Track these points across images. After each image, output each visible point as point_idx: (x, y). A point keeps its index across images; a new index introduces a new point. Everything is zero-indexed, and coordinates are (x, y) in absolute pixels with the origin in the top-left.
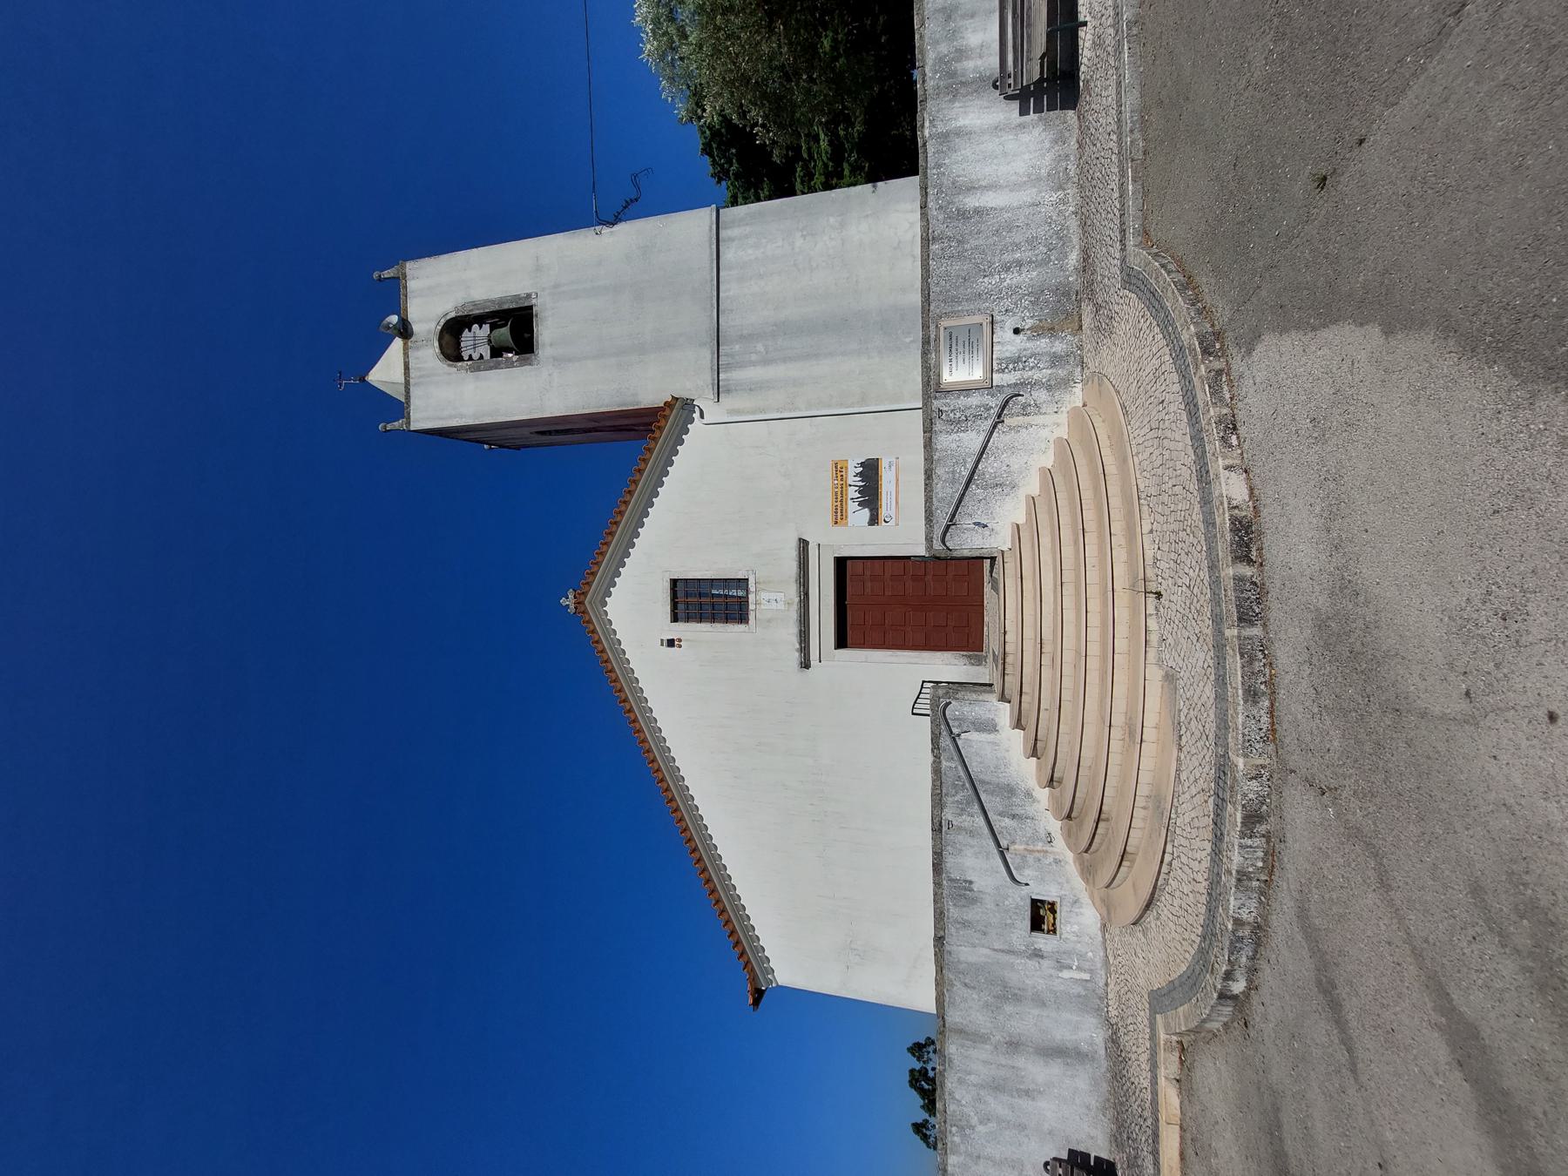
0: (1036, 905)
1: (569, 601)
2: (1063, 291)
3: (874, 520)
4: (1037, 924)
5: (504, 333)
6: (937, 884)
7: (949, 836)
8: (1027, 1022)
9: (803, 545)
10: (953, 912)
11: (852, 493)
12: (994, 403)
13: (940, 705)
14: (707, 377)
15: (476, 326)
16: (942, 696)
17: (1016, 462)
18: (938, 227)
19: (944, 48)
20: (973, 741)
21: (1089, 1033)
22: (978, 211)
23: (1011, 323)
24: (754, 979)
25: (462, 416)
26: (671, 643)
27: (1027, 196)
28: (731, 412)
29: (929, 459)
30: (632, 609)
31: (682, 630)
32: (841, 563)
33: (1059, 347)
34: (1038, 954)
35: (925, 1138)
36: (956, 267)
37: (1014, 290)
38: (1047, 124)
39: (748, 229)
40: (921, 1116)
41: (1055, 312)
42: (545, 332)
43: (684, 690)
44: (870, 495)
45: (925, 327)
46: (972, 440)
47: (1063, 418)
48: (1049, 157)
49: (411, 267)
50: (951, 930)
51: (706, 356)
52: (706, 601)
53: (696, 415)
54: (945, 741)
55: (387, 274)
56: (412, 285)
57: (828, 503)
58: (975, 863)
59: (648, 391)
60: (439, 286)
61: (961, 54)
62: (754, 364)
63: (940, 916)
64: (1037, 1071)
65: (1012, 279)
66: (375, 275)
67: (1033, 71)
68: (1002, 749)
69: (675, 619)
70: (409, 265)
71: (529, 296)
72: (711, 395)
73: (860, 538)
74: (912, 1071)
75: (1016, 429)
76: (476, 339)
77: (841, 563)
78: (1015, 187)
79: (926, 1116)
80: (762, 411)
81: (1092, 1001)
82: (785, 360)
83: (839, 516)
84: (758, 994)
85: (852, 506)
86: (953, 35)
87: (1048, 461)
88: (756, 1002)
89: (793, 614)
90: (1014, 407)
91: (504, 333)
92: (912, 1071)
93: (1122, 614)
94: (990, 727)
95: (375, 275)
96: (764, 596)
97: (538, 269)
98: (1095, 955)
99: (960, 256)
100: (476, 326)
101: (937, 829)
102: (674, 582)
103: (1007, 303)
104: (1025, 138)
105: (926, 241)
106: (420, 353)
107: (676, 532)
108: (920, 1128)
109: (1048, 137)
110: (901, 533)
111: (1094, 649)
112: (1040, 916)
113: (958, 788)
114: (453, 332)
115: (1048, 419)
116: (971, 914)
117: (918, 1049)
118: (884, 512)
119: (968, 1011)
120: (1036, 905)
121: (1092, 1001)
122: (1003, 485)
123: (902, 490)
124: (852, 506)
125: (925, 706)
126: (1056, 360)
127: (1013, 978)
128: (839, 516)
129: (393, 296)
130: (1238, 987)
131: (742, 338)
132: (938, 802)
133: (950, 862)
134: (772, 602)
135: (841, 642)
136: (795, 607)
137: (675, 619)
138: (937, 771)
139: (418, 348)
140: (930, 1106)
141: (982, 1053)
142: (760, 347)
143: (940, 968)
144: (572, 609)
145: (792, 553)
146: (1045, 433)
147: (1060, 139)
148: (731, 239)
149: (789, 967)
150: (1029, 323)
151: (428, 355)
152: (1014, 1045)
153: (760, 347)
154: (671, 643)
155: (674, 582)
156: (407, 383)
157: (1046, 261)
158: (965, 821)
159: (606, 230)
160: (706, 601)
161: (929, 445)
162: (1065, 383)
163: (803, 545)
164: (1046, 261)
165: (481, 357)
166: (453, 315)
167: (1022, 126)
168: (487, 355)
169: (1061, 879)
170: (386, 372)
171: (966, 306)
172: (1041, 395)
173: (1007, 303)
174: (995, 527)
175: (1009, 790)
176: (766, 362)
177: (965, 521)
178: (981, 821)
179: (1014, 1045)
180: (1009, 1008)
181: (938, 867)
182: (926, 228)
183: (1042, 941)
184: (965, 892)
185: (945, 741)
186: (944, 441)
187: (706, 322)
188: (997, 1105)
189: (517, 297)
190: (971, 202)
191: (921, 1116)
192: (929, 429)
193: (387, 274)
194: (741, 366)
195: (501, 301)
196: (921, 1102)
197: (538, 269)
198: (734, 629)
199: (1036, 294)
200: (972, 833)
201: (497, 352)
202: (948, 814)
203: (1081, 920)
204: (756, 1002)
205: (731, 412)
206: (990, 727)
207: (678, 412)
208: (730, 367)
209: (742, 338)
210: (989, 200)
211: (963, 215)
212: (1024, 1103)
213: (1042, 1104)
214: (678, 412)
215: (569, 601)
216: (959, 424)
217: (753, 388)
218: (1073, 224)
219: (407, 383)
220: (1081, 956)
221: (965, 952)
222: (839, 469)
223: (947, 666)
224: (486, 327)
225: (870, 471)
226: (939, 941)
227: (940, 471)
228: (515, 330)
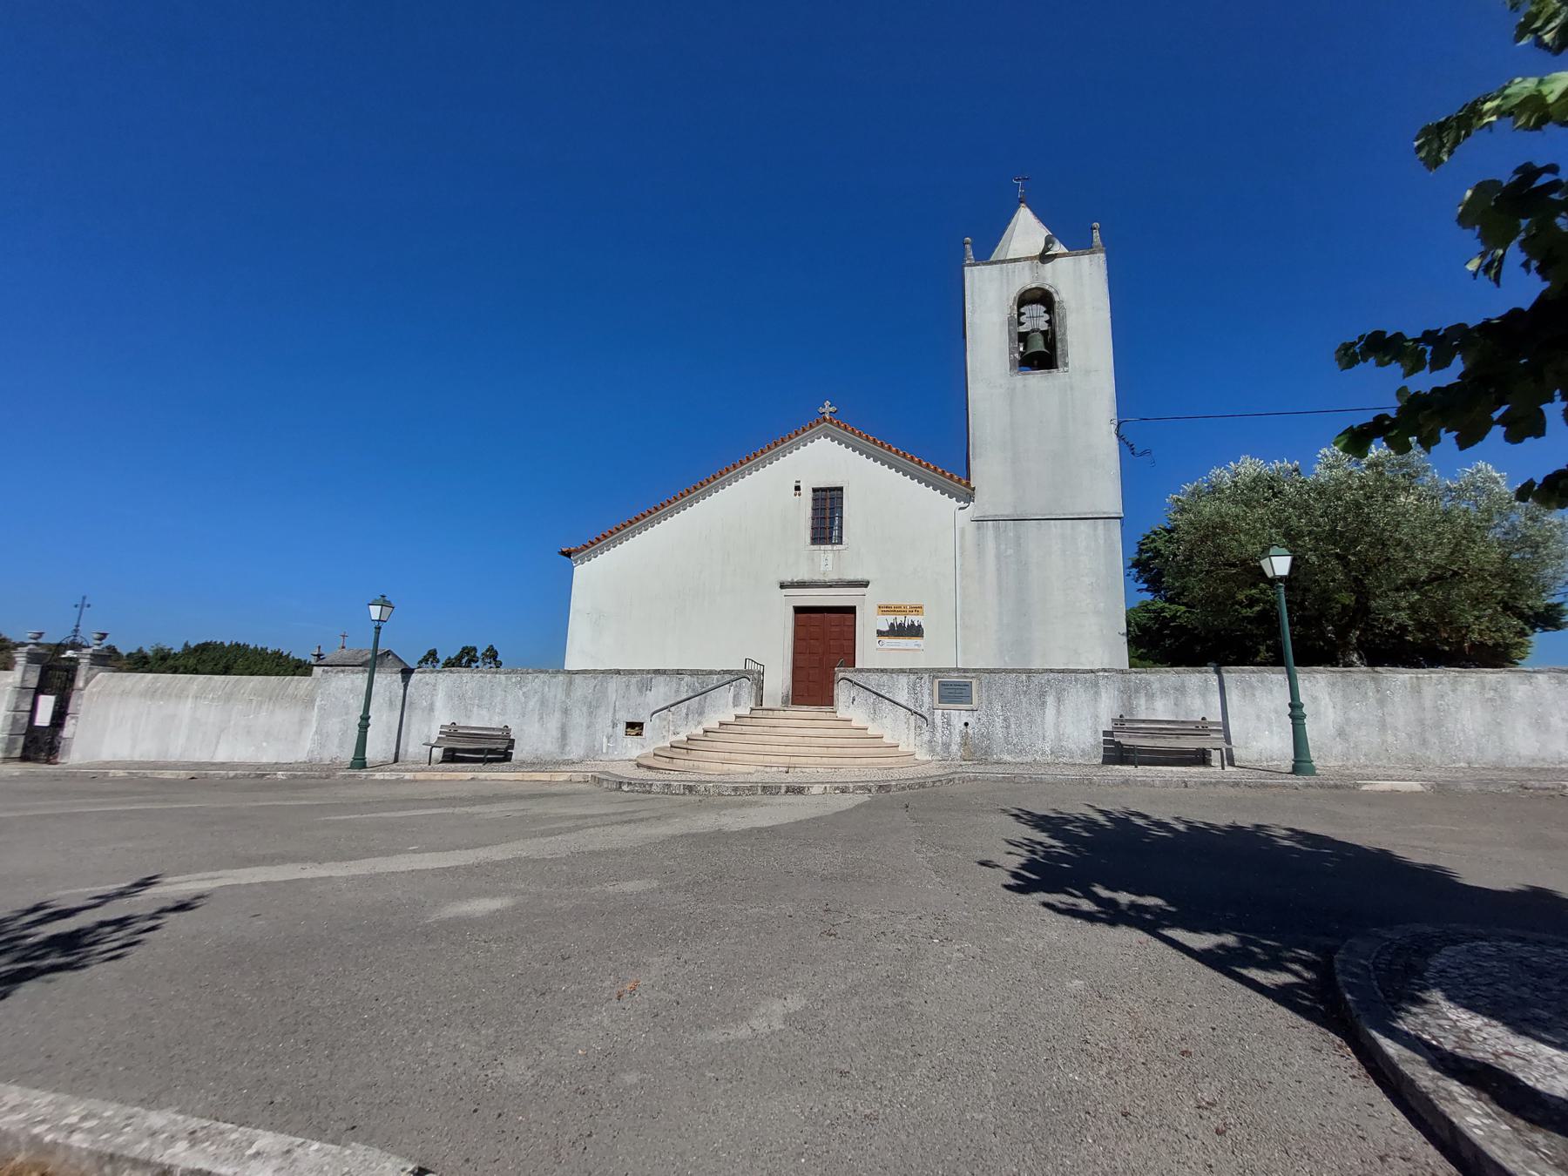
0: (641, 725)
1: (828, 408)
2: (988, 751)
3: (880, 633)
4: (631, 725)
5: (1038, 345)
6: (648, 672)
7: (675, 678)
8: (578, 718)
9: (865, 584)
10: (634, 679)
11: (900, 619)
12: (924, 711)
13: (753, 677)
14: (991, 512)
15: (1047, 317)
16: (753, 677)
17: (888, 722)
18: (1036, 679)
19: (1156, 686)
20: (727, 694)
21: (575, 751)
22: (1044, 703)
23: (971, 721)
24: (577, 551)
25: (974, 312)
26: (797, 488)
27: (1051, 733)
28: (963, 531)
29: (893, 671)
30: (822, 458)
31: (807, 496)
32: (851, 610)
33: (954, 748)
34: (614, 725)
35: (425, 660)
36: (1009, 689)
37: (992, 723)
38: (1095, 747)
39: (1102, 542)
40: (442, 658)
41: (975, 746)
42: (1037, 380)
43: (770, 492)
44: (897, 631)
45: (975, 670)
46: (903, 697)
47: (911, 749)
48: (1073, 747)
49: (1100, 258)
50: (625, 679)
51: (1007, 511)
52: (827, 515)
53: (962, 504)
54: (727, 677)
55: (1096, 234)
56: (1085, 259)
57: (894, 602)
58: (661, 692)
59: (986, 468)
60: (1082, 284)
61: (1150, 697)
62: (998, 548)
63: (631, 672)
64: (553, 723)
65: (999, 722)
66: (1096, 225)
67: (1126, 740)
68: (724, 708)
69: (814, 490)
70: (1102, 256)
71: (1066, 365)
72: (977, 515)
73: (868, 624)
74: (475, 649)
75: (907, 722)
76: (1036, 318)
77: (851, 610)
78: (1057, 725)
79: (443, 661)
80: (962, 554)
81: (592, 753)
82: (998, 570)
83: (885, 609)
84: (568, 554)
85: (891, 619)
86: (1164, 692)
87: (887, 740)
88: (563, 553)
89: (817, 577)
90: (920, 721)
91: (1038, 345)
92: (475, 649)
93: (781, 760)
94: (736, 704)
95: (1096, 225)
96: (830, 556)
97: (1087, 372)
98: (615, 755)
99: (1016, 693)
100: (1047, 317)
101: (679, 672)
102: (841, 489)
103: (984, 719)
104: (1088, 733)
105: (1029, 672)
106: (1027, 272)
107: (876, 488)
108: (432, 656)
109: (1087, 747)
110: (870, 650)
111: (768, 748)
112: (635, 727)
113: (702, 684)
114: (1042, 298)
115: (912, 741)
116: (633, 688)
117: (492, 655)
118: (886, 640)
119: (582, 687)
120: (641, 725)
121: (592, 753)
122: (875, 713)
123: (902, 652)
124: (891, 619)
125: (750, 666)
126: (946, 746)
127: (601, 711)
128: (885, 609)
129: (1078, 244)
130: (625, 788)
131: (1018, 537)
132: (694, 673)
133: (661, 678)
134: (826, 562)
135: (799, 610)
136: (822, 578)
137: (814, 490)
138: (711, 672)
139: (1031, 269)
140: (451, 664)
141: (561, 695)
142: (1010, 552)
143: (603, 672)
144: (821, 410)
145: (859, 577)
146: (904, 737)
147: (1084, 753)
148: (1095, 529)
149: (587, 573)
150: (970, 732)
151: (1025, 278)
152: (566, 712)
153: (1010, 552)
154: (797, 488)
155: (841, 489)
156: (1003, 262)
157: (1008, 743)
158: (684, 688)
159: (1113, 428)
160: (827, 515)
161: (902, 671)
162: (932, 751)
163: (865, 584)
164: (1008, 743)
165: (1021, 324)
166: (1056, 298)
167: (1096, 732)
168: (1022, 329)
169: (655, 738)
170: (1026, 232)
171: (985, 695)
172: (926, 737)
173: (984, 719)
174: (849, 705)
175: (701, 714)
176: (998, 557)
177: (854, 691)
178: (684, 696)
179: (566, 712)
180: (585, 709)
181: (657, 672)
182: (1037, 672)
183: (622, 727)
184: (645, 687)
185: (727, 677)
186: (903, 680)
187: (1033, 510)
188: (533, 703)
189: (1066, 355)
190: (1050, 700)
191: (442, 658)
192: (911, 671)
193: (1096, 234)
194: (997, 538)
195: (1064, 341)
196: (192, 645)
197: (1087, 372)
198: (807, 535)
199: (988, 737)
200: (677, 691)
201: (1023, 338)
202: (687, 678)
203: (634, 748)
204: (563, 553)
205: (963, 531)
206: (736, 704)
207: (966, 494)
208: (997, 529)
209: (1018, 537)
210: (1050, 711)
211: (1042, 695)
212: (536, 717)
213: (537, 725)
214: (966, 494)
215: (828, 408)
216: (913, 689)
217: (980, 545)
218: (1029, 759)
219: (1003, 262)
220: (615, 748)
221: (614, 684)
222: (917, 609)
223: (778, 679)
224: (1045, 327)
225: (915, 631)
226: (618, 672)
227: (885, 677)
228: (1039, 354)
